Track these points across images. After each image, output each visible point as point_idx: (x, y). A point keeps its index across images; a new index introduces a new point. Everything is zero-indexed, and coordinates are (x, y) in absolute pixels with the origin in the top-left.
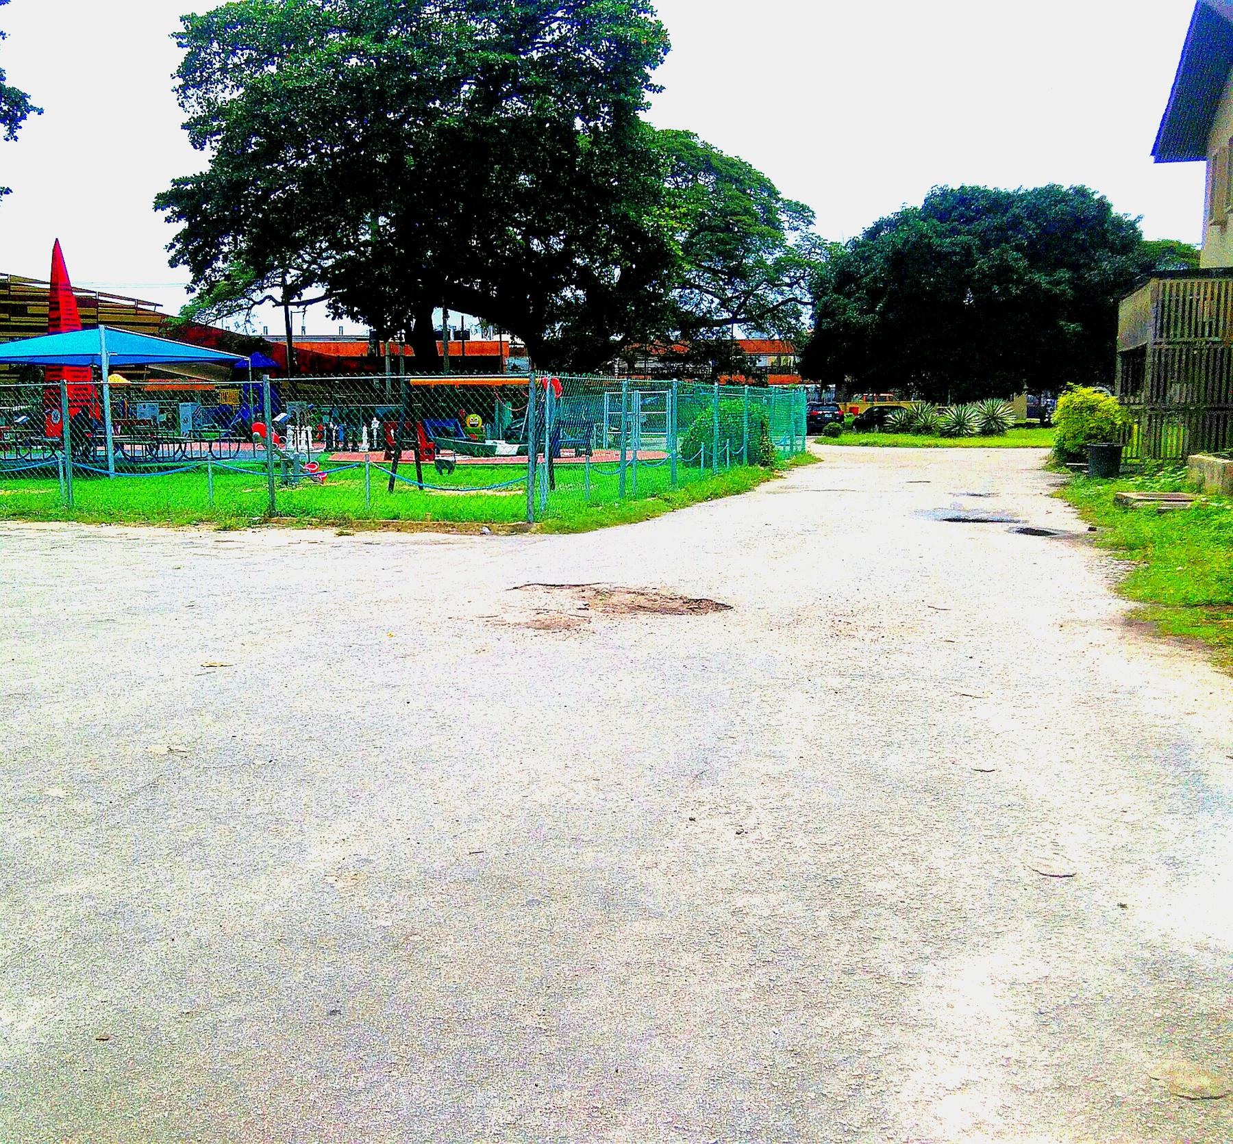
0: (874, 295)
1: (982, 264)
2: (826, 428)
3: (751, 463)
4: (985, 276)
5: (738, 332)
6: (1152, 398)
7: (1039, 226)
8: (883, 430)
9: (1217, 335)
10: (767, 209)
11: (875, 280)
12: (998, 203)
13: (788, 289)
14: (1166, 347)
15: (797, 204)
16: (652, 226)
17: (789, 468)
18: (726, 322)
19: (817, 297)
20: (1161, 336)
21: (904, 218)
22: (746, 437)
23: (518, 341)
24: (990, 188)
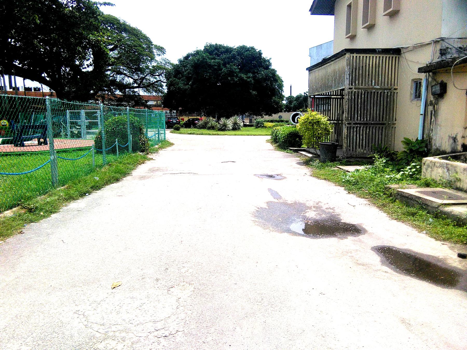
0: (188, 79)
2: (174, 127)
3: (134, 150)
4: (226, 74)
5: (141, 92)
6: (348, 118)
7: (242, 58)
8: (195, 127)
9: (378, 85)
11: (189, 73)
12: (228, 50)
14: (354, 90)
15: (159, 46)
17: (156, 151)
19: (168, 79)
20: (352, 85)
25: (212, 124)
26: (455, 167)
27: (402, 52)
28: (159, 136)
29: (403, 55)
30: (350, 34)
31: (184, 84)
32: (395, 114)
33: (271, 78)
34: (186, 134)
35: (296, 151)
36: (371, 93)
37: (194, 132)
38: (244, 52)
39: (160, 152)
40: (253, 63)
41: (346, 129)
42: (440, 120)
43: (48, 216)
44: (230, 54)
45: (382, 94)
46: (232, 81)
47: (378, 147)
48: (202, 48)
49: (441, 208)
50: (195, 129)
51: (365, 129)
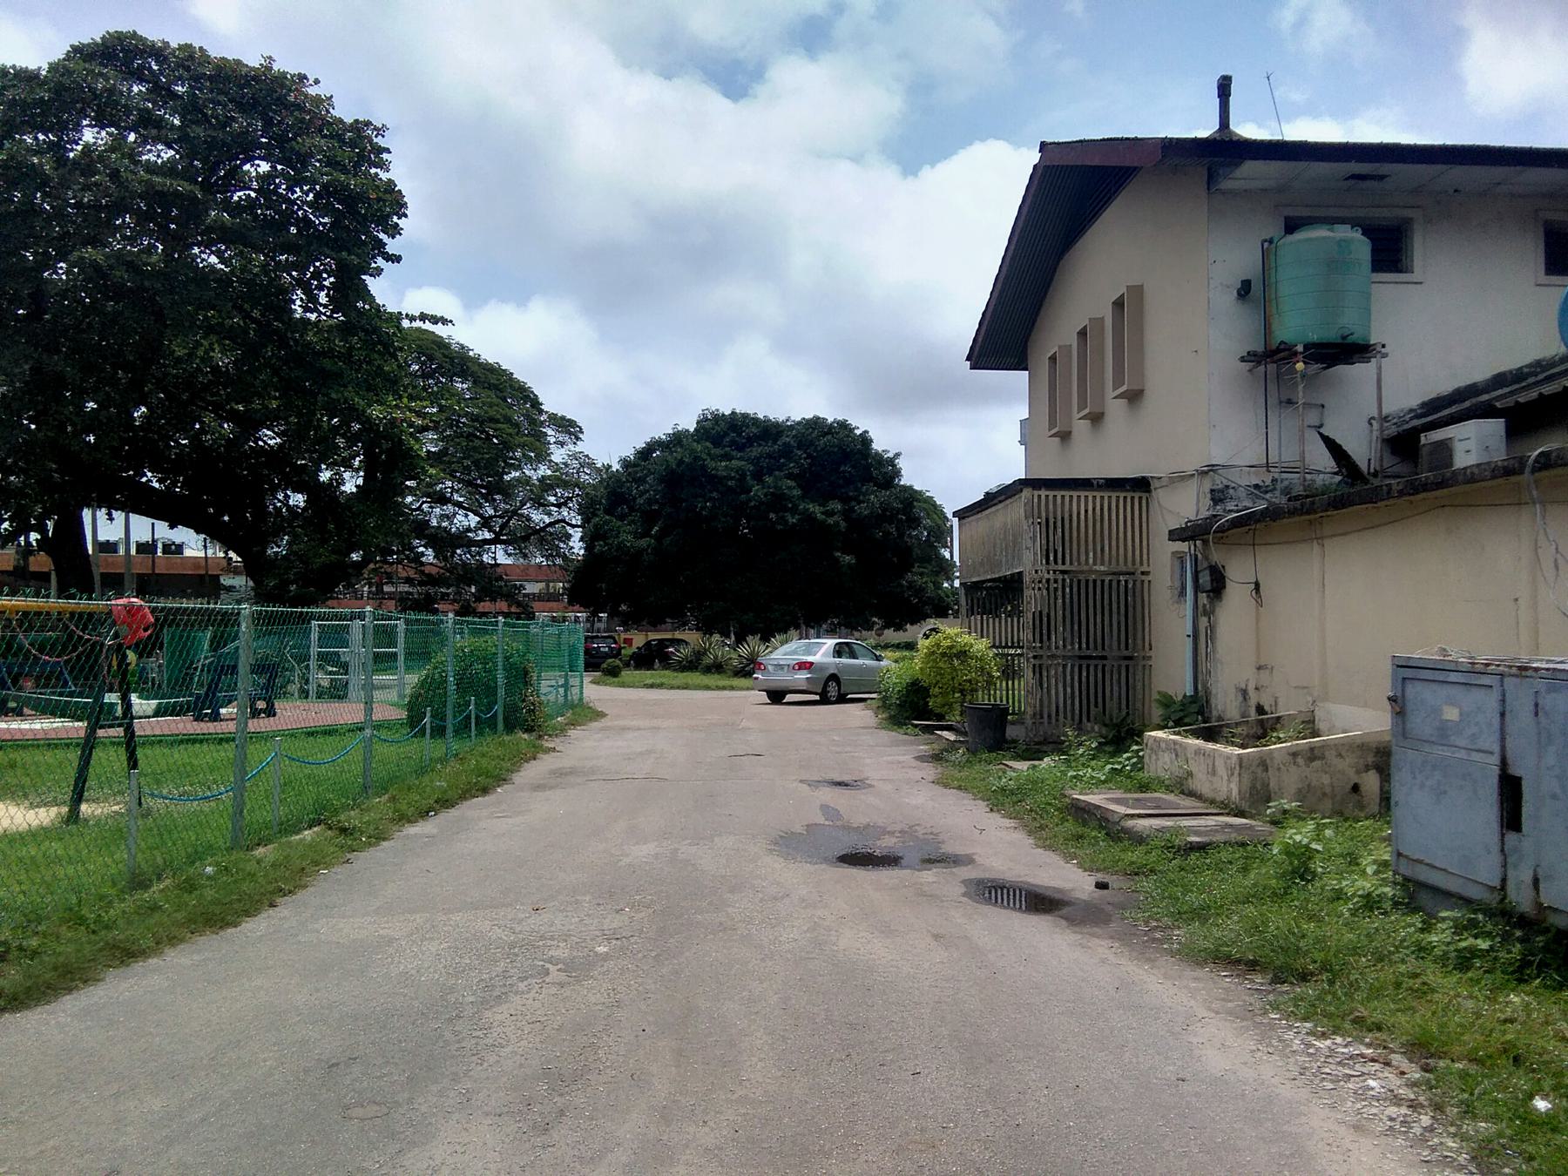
0: (649, 518)
1: (756, 490)
2: (604, 666)
3: (510, 727)
4: (762, 503)
5: (501, 556)
7: (809, 456)
9: (1102, 564)
10: (533, 422)
11: (650, 502)
13: (556, 509)
15: (563, 418)
16: (385, 418)
17: (562, 731)
18: (486, 542)
19: (586, 520)
21: (678, 439)
22: (501, 692)
23: (232, 554)
24: (761, 416)
25: (716, 657)
26: (1184, 747)
27: (1152, 488)
28: (566, 691)
29: (1154, 493)
30: (1124, 388)
31: (636, 533)
32: (1147, 630)
33: (898, 513)
34: (638, 687)
35: (928, 730)
36: (1087, 581)
37: (664, 680)
38: (818, 438)
39: (572, 733)
40: (844, 472)
41: (1031, 670)
42: (1220, 651)
43: (376, 844)
44: (775, 442)
45: (1114, 584)
46: (780, 524)
47: (1041, 711)
48: (691, 425)
49: (1130, 823)
50: (667, 672)
51: (1076, 670)
